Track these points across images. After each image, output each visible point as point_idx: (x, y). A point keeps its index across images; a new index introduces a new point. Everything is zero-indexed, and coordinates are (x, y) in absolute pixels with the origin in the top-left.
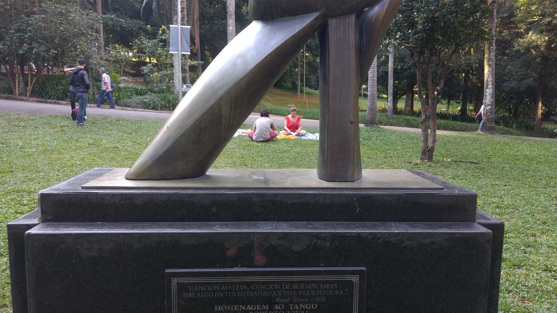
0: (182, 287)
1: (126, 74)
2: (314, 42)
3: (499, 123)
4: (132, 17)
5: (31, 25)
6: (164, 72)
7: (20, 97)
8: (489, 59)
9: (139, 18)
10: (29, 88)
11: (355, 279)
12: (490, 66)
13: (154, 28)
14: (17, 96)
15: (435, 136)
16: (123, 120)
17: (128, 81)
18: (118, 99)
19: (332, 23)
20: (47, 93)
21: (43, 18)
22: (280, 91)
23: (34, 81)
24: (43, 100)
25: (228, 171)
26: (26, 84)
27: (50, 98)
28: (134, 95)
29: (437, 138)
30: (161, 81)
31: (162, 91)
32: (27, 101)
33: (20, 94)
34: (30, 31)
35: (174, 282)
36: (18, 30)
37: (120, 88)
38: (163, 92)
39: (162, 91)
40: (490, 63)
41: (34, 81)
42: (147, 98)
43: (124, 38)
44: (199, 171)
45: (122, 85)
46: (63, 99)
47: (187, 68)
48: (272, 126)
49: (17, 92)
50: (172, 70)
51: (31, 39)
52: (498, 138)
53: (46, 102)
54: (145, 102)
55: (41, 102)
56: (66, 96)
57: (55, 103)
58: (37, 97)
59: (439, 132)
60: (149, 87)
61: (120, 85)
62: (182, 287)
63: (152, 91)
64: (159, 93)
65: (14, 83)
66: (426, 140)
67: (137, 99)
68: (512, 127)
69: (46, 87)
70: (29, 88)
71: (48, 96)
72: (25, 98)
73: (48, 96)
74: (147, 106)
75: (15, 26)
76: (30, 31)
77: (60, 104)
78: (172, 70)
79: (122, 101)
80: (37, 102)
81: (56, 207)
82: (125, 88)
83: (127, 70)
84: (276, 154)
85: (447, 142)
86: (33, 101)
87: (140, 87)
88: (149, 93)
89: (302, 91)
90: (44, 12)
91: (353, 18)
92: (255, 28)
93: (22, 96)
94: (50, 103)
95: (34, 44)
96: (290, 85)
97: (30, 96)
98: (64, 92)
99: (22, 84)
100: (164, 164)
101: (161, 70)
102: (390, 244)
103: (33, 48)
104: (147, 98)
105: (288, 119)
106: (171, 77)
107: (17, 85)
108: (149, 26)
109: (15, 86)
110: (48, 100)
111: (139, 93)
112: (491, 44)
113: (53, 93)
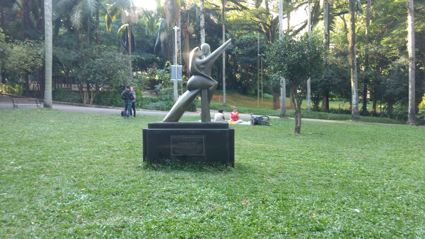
0: (173, 139)
1: (145, 89)
2: (200, 93)
3: (387, 116)
4: (148, 52)
5: (95, 64)
6: (168, 88)
7: (87, 105)
8: (354, 78)
9: (153, 53)
10: (92, 99)
11: (203, 138)
12: (354, 82)
13: (161, 59)
14: (85, 104)
15: (300, 121)
16: (147, 116)
17: (147, 94)
18: (142, 104)
19: (203, 91)
20: (102, 102)
21: (102, 61)
22: (246, 97)
23: (94, 95)
24: (99, 106)
25: (181, 121)
26: (90, 97)
27: (103, 105)
28: (151, 102)
29: (302, 122)
30: (166, 94)
31: (167, 100)
32: (91, 107)
33: (87, 103)
34: (95, 68)
35: (172, 138)
36: (88, 68)
37: (142, 98)
38: (167, 100)
39: (167, 100)
40: (354, 80)
41: (94, 95)
42: (158, 104)
43: (141, 65)
44: (177, 120)
45: (144, 97)
46: (110, 105)
47: (182, 85)
48: (223, 118)
49: (85, 102)
50: (172, 87)
51: (95, 72)
52: (359, 124)
53: (101, 107)
54: (157, 107)
55: (98, 107)
56: (112, 103)
57: (106, 108)
58: (96, 104)
59: (302, 119)
60: (159, 97)
61: (143, 97)
62: (173, 139)
63: (161, 100)
64: (165, 101)
65: (84, 96)
66: (297, 123)
67: (152, 104)
68: (395, 119)
69: (101, 98)
70: (92, 99)
71: (102, 104)
72: (89, 105)
73: (102, 104)
74: (158, 109)
75: (86, 65)
76: (95, 68)
77: (108, 108)
78: (172, 87)
79: (144, 106)
80: (96, 107)
81: (150, 126)
82: (145, 98)
83: (146, 87)
84: (192, 117)
85: (308, 123)
86: (94, 107)
87: (154, 97)
88: (159, 101)
89: (260, 96)
90: (103, 57)
91: (207, 90)
92: (188, 92)
93: (88, 104)
94: (103, 108)
95: (97, 75)
96: (253, 92)
97: (92, 104)
98: (111, 101)
99: (88, 97)
100: (169, 119)
101: (166, 87)
102: (209, 131)
103: (96, 77)
104: (158, 104)
105: (232, 114)
106: (172, 91)
107: (85, 98)
108: (158, 58)
109: (84, 98)
110: (102, 106)
111: (154, 101)
112: (354, 69)
113: (105, 102)
